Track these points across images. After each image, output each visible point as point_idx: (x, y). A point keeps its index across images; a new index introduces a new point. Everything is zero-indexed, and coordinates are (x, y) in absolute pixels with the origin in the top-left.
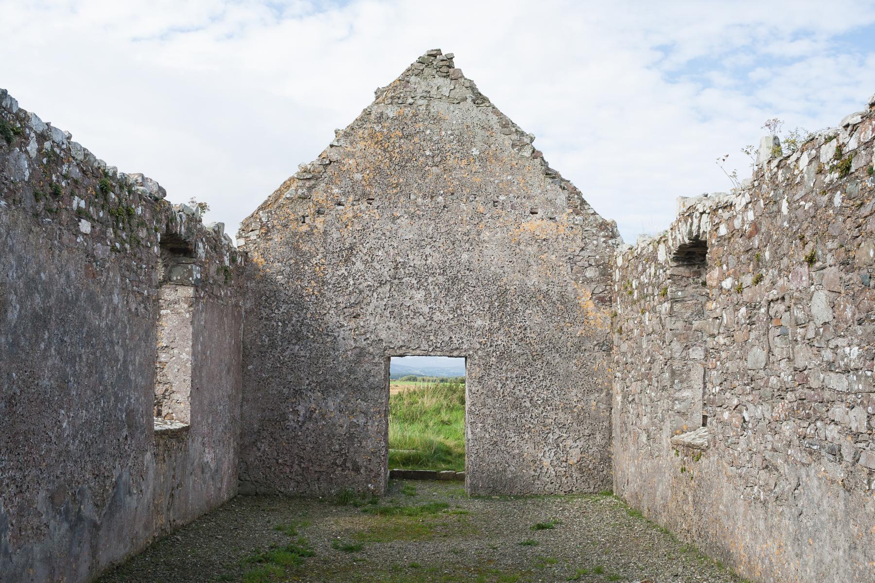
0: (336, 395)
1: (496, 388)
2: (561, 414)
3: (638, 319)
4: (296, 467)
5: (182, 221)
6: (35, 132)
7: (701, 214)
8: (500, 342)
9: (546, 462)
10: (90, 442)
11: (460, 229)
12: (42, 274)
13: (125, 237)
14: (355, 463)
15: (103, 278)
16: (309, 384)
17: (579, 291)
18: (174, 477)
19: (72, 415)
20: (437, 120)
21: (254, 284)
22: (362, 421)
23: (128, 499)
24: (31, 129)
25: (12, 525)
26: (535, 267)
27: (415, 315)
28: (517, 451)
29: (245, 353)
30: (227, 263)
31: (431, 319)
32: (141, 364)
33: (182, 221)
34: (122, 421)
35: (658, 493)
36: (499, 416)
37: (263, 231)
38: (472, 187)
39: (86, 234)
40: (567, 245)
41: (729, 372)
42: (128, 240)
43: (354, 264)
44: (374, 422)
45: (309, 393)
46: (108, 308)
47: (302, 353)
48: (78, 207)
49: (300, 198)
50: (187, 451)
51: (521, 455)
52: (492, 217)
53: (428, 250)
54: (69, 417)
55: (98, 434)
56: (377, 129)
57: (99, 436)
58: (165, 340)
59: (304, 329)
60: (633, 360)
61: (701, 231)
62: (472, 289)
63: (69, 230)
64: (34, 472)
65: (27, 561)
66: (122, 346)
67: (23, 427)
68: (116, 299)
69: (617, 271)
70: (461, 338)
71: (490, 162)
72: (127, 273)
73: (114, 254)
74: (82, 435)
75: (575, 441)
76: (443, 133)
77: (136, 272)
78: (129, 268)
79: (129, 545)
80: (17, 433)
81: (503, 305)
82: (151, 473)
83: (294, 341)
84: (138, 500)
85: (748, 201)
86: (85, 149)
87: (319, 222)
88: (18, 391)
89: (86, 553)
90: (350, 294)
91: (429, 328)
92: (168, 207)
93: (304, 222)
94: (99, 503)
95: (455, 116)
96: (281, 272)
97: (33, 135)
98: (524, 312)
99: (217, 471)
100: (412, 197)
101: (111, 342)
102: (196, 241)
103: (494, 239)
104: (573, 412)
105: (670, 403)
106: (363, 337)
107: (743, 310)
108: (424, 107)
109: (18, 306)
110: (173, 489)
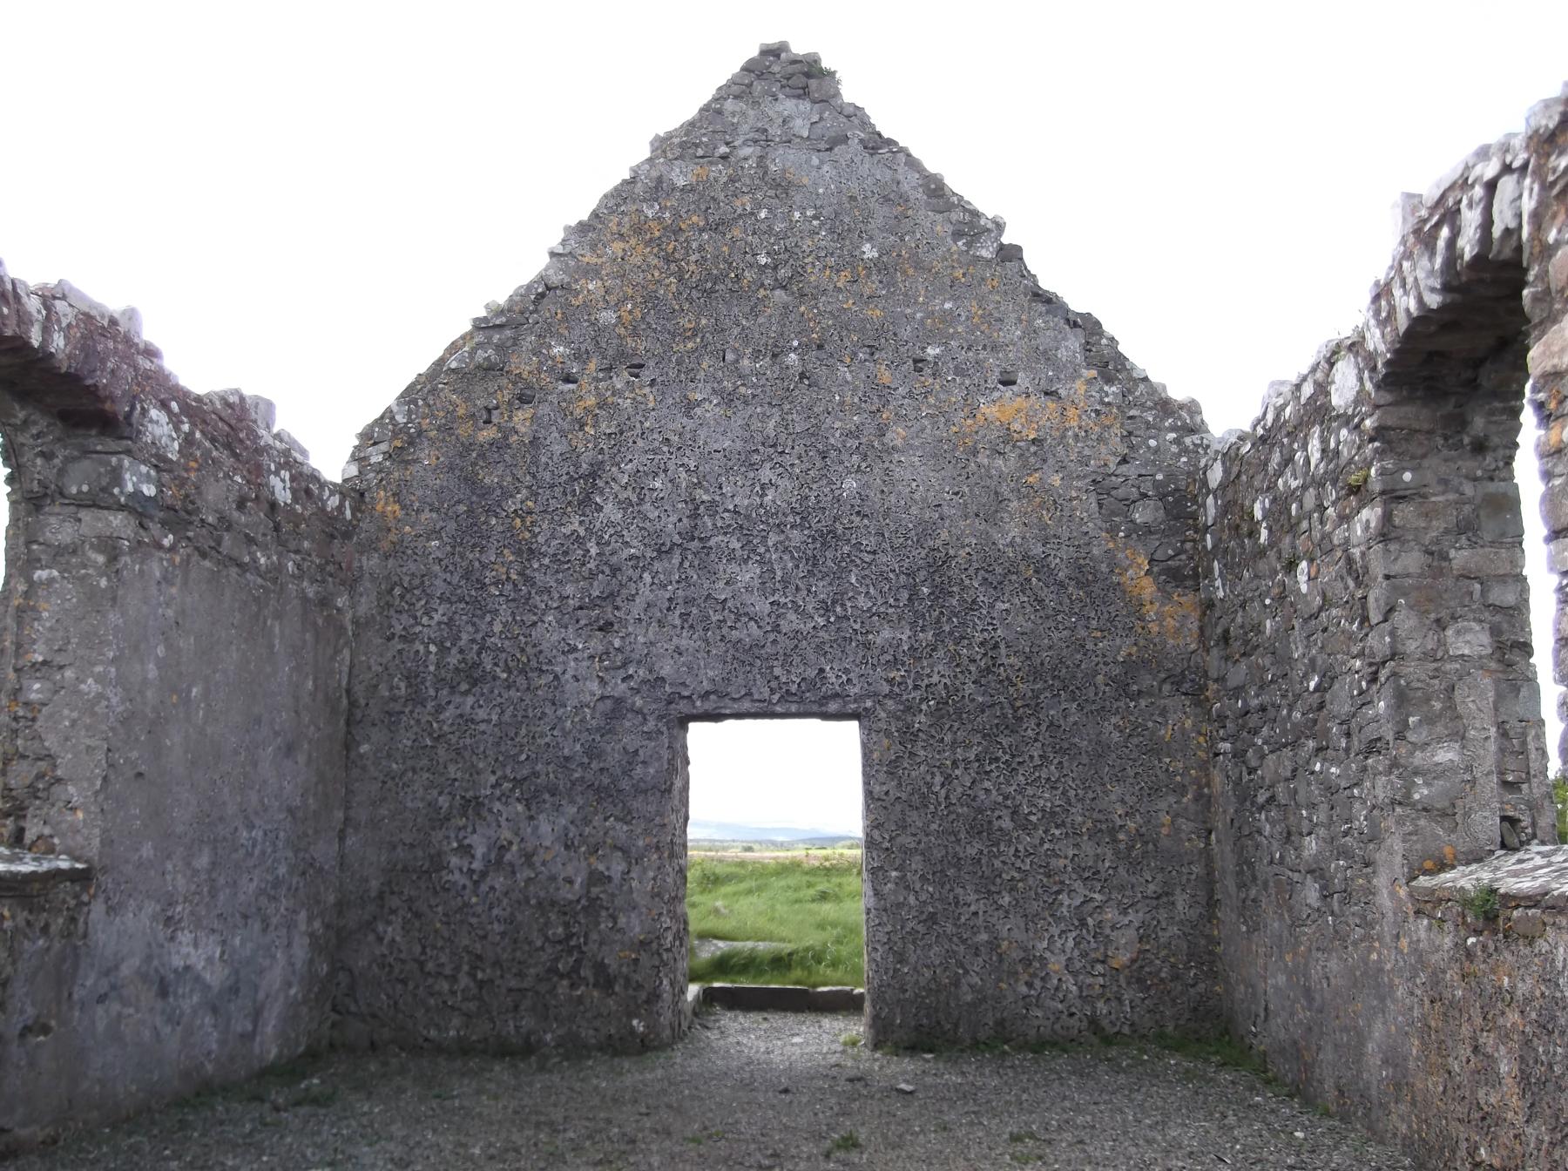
0: (558, 808)
1: (929, 785)
2: (1088, 848)
4: (464, 981)
8: (935, 679)
9: (1056, 964)
11: (837, 424)
14: (600, 967)
20: (783, 187)
22: (617, 867)
28: (984, 937)
29: (349, 716)
31: (776, 628)
36: (938, 854)
38: (863, 330)
40: (1087, 452)
43: (600, 509)
44: (645, 870)
45: (497, 806)
49: (479, 367)
51: (994, 945)
52: (910, 395)
53: (766, 474)
61: (1497, 232)
62: (868, 558)
69: (1210, 500)
70: (847, 671)
71: (904, 272)
75: (1124, 912)
76: (797, 215)
90: (592, 576)
91: (769, 649)
93: (488, 422)
96: (435, 533)
98: (992, 606)
100: (730, 357)
104: (1115, 841)
105: (1399, 783)
106: (622, 673)
108: (752, 162)
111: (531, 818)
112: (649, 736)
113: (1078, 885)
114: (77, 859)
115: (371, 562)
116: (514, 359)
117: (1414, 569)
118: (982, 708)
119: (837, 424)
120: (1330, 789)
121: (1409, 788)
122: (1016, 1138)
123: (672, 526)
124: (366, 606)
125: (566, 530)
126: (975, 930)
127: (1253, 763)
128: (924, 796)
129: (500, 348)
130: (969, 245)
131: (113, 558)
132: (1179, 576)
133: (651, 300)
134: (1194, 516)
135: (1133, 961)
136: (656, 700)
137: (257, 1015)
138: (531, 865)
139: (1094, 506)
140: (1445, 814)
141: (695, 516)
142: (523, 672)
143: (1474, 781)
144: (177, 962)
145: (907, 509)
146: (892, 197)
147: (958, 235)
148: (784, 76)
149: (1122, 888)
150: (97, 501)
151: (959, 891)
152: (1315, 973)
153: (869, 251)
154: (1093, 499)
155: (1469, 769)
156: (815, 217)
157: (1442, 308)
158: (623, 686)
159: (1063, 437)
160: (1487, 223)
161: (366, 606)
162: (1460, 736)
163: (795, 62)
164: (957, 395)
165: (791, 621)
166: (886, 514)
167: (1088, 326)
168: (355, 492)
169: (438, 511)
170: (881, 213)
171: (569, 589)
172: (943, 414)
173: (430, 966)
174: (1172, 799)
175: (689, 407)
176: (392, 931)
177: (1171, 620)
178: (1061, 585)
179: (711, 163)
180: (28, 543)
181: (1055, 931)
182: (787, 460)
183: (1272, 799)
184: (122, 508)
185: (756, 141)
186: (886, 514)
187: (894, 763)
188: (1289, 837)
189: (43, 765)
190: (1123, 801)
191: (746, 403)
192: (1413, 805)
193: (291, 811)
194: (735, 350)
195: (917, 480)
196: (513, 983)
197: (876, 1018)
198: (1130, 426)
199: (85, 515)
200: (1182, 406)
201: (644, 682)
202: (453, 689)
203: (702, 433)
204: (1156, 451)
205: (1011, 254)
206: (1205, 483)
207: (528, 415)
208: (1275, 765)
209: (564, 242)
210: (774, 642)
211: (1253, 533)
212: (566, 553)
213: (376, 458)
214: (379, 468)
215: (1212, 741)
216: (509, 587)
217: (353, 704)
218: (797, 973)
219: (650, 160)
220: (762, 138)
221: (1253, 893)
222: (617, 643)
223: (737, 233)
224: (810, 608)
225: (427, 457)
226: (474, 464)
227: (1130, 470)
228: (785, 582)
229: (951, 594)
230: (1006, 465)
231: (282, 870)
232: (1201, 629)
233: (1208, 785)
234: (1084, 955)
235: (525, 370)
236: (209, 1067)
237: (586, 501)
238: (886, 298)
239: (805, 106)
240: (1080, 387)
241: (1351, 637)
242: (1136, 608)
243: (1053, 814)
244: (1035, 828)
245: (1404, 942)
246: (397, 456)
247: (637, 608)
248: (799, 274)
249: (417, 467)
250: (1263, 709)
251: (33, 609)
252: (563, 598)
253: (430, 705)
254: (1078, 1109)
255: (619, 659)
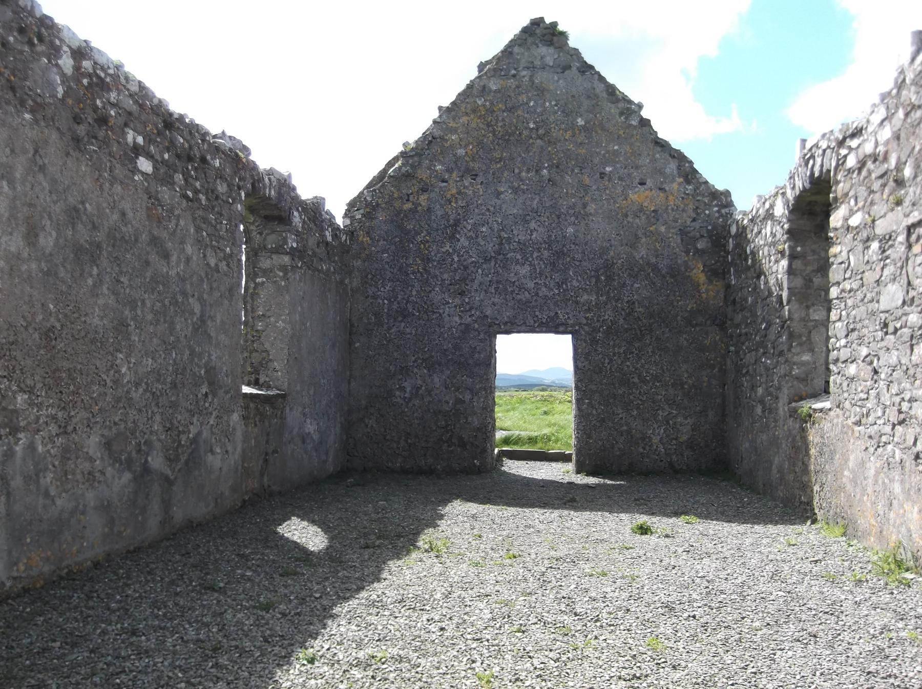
0: (442, 371)
1: (603, 363)
2: (671, 391)
3: (753, 286)
4: (403, 443)
5: (271, 184)
6: (69, 47)
7: (824, 151)
8: (607, 317)
9: (656, 440)
10: (158, 393)
11: (565, 203)
12: (87, 205)
13: (199, 187)
14: (461, 439)
15: (172, 225)
16: (415, 361)
17: (690, 263)
18: (267, 442)
19: (133, 361)
20: (541, 91)
21: (359, 263)
22: (468, 397)
23: (210, 457)
24: (61, 40)
25: (54, 466)
26: (644, 240)
27: (520, 291)
28: (625, 428)
29: (350, 332)
30: (329, 239)
31: (537, 294)
32: (222, 322)
33: (271, 184)
34: (200, 377)
35: (774, 467)
36: (606, 393)
37: (368, 210)
38: (577, 159)
39: (147, 174)
40: (677, 216)
41: (857, 320)
42: (204, 191)
43: (458, 240)
44: (479, 398)
45: (415, 370)
46: (179, 257)
47: (408, 330)
48: (134, 142)
49: (403, 175)
50: (283, 418)
51: (629, 432)
52: (598, 189)
53: (533, 225)
54: (129, 363)
55: (169, 386)
56: (480, 103)
57: (171, 388)
58: (261, 308)
59: (410, 307)
60: (747, 330)
61: (824, 171)
62: (578, 263)
63: (124, 165)
64: (83, 414)
65: (77, 507)
66: (199, 299)
67: (66, 364)
68: (189, 249)
69: (731, 240)
70: (567, 314)
71: (596, 132)
72: (204, 226)
73: (184, 201)
74: (147, 384)
75: (686, 419)
76: (547, 104)
77: (215, 227)
78: (205, 220)
79: (212, 505)
80: (57, 370)
81: (610, 279)
82: (239, 434)
83: (400, 319)
84: (222, 460)
85: (883, 117)
86: (140, 82)
87: (423, 199)
88: (58, 326)
89: (156, 507)
90: (456, 270)
91: (533, 303)
92: (253, 167)
93: (408, 200)
94: (172, 457)
95: (558, 84)
96: (385, 251)
97: (65, 48)
98: (632, 285)
99: (321, 443)
100: (517, 171)
101: (184, 294)
102: (290, 209)
103: (600, 211)
104: (683, 388)
105: (788, 368)
106: (469, 313)
107: (875, 245)
108: (527, 78)
109: (54, 234)
110: (267, 454)
111: (430, 375)
112: (481, 341)
113: (666, 407)
114: (269, 387)
115: (358, 263)
116: (419, 171)
117: (798, 286)
118: (627, 330)
119: (565, 203)
120: (767, 369)
121: (792, 369)
122: (636, 500)
123: (490, 248)
124: (356, 283)
125: (444, 250)
126: (621, 425)
127: (742, 357)
128: (600, 368)
129: (412, 166)
130: (626, 118)
131: (286, 274)
132: (717, 273)
133: (480, 144)
134: (724, 246)
135: (689, 439)
136: (484, 325)
137: (327, 454)
138: (430, 396)
139: (679, 241)
140: (803, 380)
141: (501, 244)
142: (426, 312)
143: (815, 368)
144: (307, 431)
145: (596, 241)
146: (591, 95)
147: (621, 114)
148: (542, 34)
149: (685, 408)
150: (278, 250)
151: (614, 408)
152: (759, 441)
153: (580, 122)
154: (679, 238)
155: (814, 363)
156: (556, 105)
157: (811, 188)
158: (469, 319)
159: (667, 209)
160: (822, 166)
161: (356, 283)
162: (811, 350)
163: (546, 28)
164: (619, 190)
165: (544, 291)
166: (586, 244)
167: (680, 157)
168: (351, 232)
169: (387, 241)
170: (586, 103)
171: (445, 276)
172: (613, 198)
173: (388, 437)
174: (709, 371)
175: (498, 194)
176: (372, 422)
177: (710, 292)
178: (664, 277)
179: (508, 79)
180: (254, 268)
181: (655, 426)
182: (542, 219)
183: (748, 371)
184: (287, 253)
185: (528, 68)
186: (586, 244)
187: (588, 354)
188: (753, 388)
189: (264, 355)
190: (687, 371)
191: (524, 193)
192: (792, 376)
193: (334, 371)
194: (519, 168)
195: (600, 229)
196: (423, 445)
197: (577, 461)
198: (697, 204)
199: (274, 257)
200: (722, 193)
201: (479, 317)
202: (395, 320)
203: (504, 206)
204: (709, 215)
205: (645, 123)
206: (729, 232)
207: (426, 197)
208: (749, 358)
209: (440, 116)
210: (536, 301)
211: (746, 260)
212: (444, 260)
213: (358, 216)
214: (360, 221)
215: (727, 346)
216: (419, 275)
217: (352, 325)
218: (540, 445)
219: (479, 77)
220: (531, 67)
221: (740, 410)
222: (467, 300)
223: (520, 112)
224: (552, 285)
225: (381, 216)
226: (402, 220)
227: (697, 225)
228: (541, 274)
229: (614, 280)
230: (640, 222)
231: (332, 396)
232: (725, 297)
233: (725, 365)
234: (668, 436)
235: (424, 177)
236: (315, 472)
237: (452, 238)
238: (588, 144)
239: (551, 50)
240: (675, 186)
241: (776, 310)
242: (696, 287)
243: (656, 376)
244: (648, 382)
245: (786, 427)
246: (368, 216)
247: (476, 285)
248: (548, 132)
249: (377, 221)
250: (746, 334)
251: (257, 294)
252: (443, 280)
253: (386, 326)
254: (661, 492)
255: (468, 307)
